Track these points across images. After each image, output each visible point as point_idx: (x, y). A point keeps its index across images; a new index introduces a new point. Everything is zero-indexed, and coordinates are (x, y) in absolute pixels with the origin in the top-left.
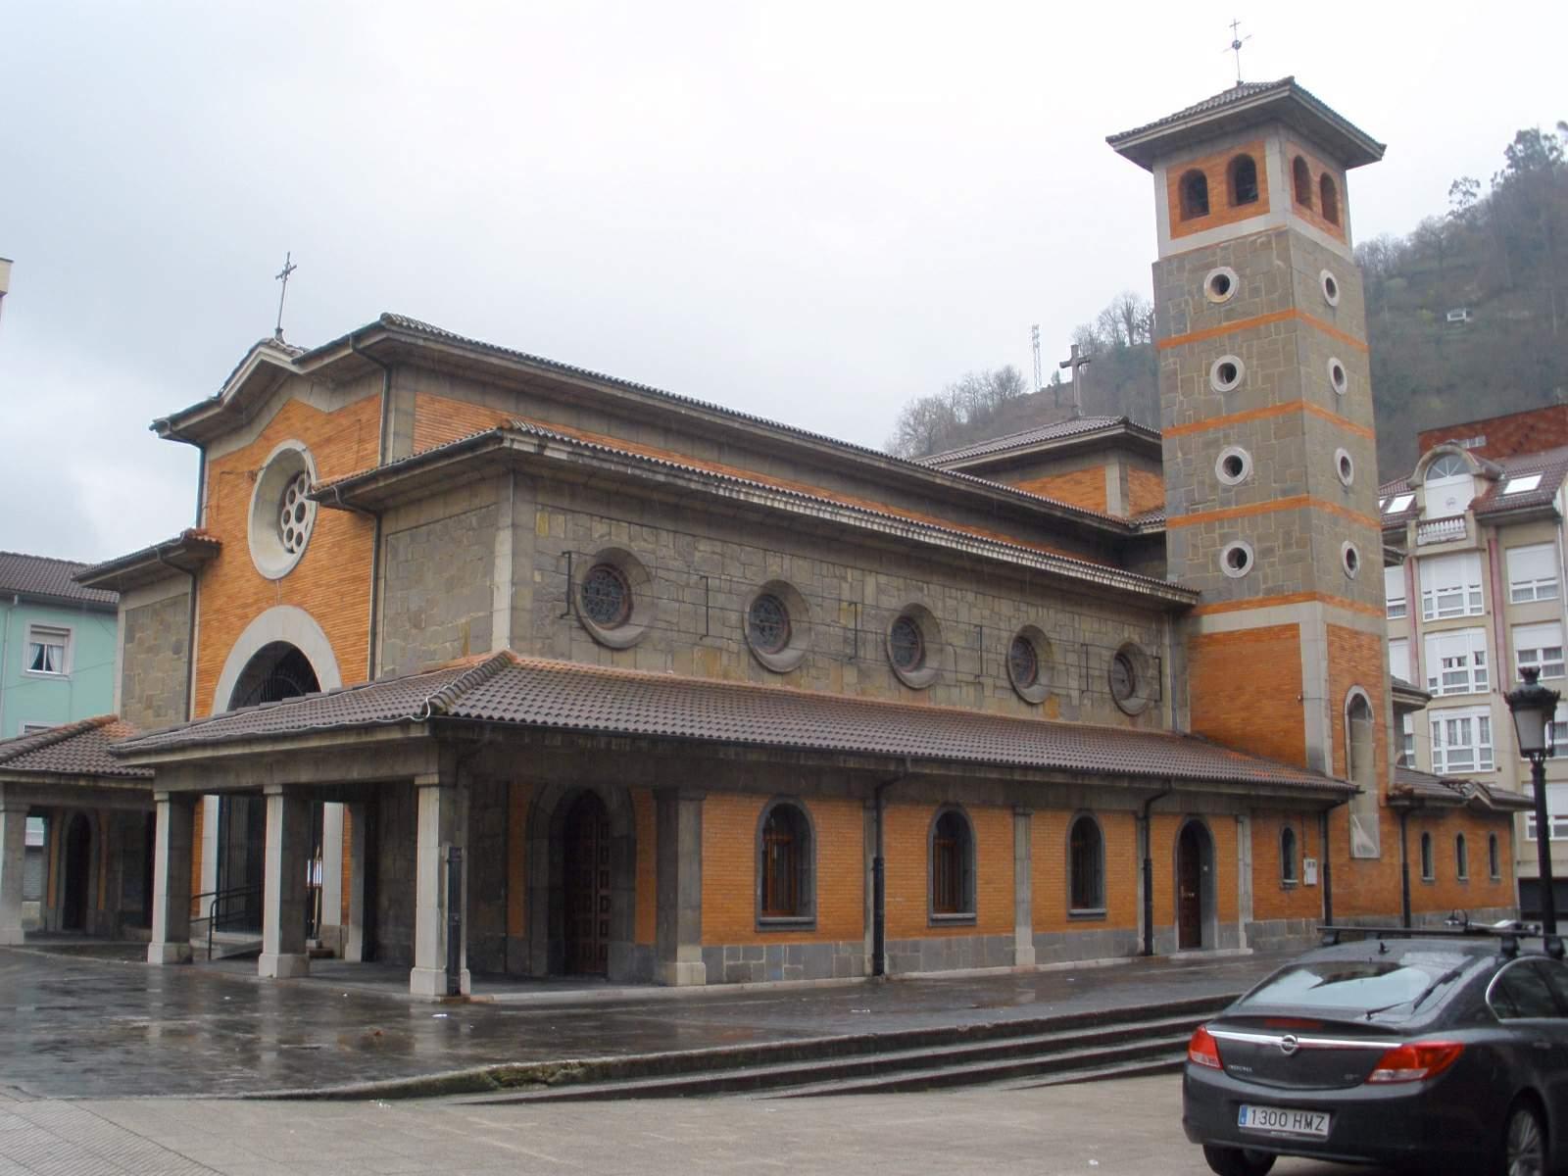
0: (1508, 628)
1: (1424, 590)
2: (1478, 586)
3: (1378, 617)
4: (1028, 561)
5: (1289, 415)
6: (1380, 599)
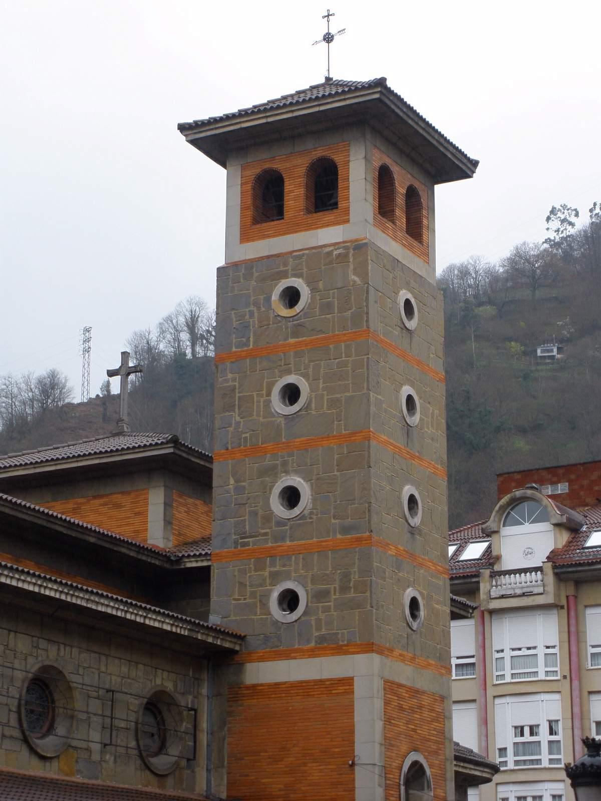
0: (585, 694)
1: (496, 647)
2: (554, 647)
3: (442, 675)
4: (51, 591)
5: (356, 449)
6: (444, 656)
